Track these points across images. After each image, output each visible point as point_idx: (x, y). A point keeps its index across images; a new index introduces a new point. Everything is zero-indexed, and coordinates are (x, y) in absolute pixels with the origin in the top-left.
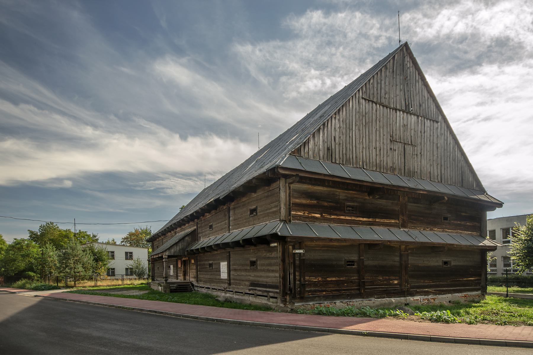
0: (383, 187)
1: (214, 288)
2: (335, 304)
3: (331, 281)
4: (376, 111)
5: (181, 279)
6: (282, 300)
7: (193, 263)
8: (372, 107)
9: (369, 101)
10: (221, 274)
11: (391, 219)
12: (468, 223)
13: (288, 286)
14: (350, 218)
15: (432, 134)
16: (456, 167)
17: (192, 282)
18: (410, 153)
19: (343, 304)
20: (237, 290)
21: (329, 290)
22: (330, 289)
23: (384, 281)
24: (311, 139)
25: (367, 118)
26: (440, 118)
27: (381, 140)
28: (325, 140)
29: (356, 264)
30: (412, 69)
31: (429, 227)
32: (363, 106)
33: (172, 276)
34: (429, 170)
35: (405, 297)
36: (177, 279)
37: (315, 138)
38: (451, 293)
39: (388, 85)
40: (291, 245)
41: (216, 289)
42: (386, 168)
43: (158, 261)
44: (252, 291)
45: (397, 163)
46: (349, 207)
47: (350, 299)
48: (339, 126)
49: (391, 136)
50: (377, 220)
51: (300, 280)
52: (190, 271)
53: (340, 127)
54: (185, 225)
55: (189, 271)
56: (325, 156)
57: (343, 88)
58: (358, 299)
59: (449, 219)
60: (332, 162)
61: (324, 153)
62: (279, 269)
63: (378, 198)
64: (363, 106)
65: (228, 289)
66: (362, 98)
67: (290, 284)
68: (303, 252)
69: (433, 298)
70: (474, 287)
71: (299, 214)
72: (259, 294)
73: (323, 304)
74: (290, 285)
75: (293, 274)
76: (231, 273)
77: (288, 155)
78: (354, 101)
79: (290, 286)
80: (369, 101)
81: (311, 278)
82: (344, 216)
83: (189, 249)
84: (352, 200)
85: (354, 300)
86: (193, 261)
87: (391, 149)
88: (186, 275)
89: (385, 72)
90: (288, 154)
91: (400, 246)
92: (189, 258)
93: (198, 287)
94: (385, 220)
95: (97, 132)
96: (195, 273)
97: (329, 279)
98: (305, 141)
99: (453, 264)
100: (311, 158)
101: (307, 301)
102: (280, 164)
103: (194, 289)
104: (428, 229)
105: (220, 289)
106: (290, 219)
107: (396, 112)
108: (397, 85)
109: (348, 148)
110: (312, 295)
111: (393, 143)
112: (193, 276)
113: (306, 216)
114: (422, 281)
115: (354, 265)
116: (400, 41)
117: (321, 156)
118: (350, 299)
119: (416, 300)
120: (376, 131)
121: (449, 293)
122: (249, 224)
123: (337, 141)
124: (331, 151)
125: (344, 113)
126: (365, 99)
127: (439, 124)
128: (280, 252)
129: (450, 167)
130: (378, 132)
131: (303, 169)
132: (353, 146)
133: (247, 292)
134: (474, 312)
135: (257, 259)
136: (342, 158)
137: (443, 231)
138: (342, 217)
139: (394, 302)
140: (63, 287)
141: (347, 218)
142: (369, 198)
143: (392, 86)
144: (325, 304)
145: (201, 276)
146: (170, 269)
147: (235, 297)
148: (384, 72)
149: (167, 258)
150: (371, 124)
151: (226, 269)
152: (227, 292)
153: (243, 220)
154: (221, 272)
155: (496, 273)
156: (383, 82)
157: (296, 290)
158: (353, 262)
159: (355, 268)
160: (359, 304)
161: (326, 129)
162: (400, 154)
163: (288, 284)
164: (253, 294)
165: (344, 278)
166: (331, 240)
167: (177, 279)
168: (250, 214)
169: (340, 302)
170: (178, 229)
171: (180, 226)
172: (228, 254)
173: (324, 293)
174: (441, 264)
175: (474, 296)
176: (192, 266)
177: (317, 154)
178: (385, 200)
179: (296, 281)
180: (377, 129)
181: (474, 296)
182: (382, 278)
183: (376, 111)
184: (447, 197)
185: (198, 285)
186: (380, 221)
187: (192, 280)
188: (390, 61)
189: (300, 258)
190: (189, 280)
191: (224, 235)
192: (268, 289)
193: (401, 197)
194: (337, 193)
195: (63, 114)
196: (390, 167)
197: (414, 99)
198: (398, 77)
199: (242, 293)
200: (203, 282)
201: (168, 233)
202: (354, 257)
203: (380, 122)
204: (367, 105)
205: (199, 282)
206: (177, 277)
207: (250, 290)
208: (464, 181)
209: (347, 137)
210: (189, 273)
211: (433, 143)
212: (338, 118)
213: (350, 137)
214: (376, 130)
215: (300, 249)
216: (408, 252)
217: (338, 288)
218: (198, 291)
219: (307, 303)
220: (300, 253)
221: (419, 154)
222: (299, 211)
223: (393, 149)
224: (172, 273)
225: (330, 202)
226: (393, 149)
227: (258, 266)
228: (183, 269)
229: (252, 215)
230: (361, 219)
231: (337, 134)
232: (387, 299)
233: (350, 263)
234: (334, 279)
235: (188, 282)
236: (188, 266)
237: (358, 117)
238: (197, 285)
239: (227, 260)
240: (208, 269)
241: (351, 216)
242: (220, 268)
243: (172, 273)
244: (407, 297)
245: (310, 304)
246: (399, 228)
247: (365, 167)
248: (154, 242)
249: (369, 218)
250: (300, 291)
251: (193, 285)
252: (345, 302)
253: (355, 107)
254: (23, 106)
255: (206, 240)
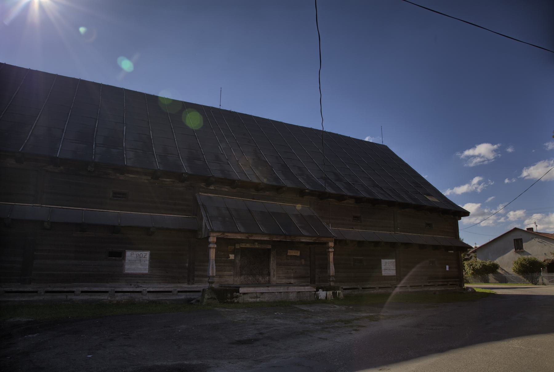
207: (429, 282)
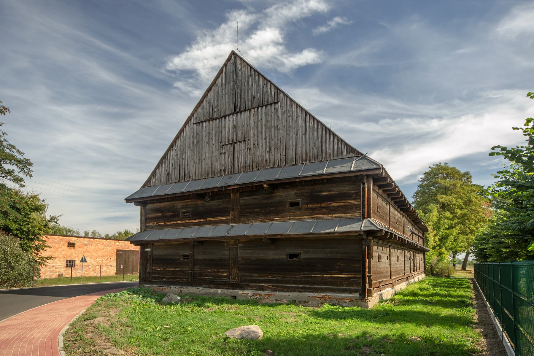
0: (193, 194)
3: (169, 270)
11: (222, 217)
12: (333, 204)
23: (211, 273)
31: (267, 218)
38: (299, 292)
50: (208, 220)
60: (169, 183)
63: (210, 200)
84: (187, 207)
95: (443, 122)
97: (167, 269)
99: (303, 256)
101: (153, 284)
114: (257, 275)
118: (182, 285)
119: (245, 294)
134: (127, 302)
137: (289, 219)
138: (179, 222)
140: (519, 265)
141: (183, 222)
174: (284, 257)
175: (339, 299)
178: (216, 201)
181: (339, 299)
184: (267, 184)
194: (176, 205)
195: (410, 116)
202: (187, 252)
216: (237, 245)
217: (174, 277)
222: (151, 222)
225: (171, 212)
230: (194, 221)
232: (214, 289)
233: (186, 257)
234: (171, 269)
241: (185, 220)
249: (200, 219)
254: (382, 122)
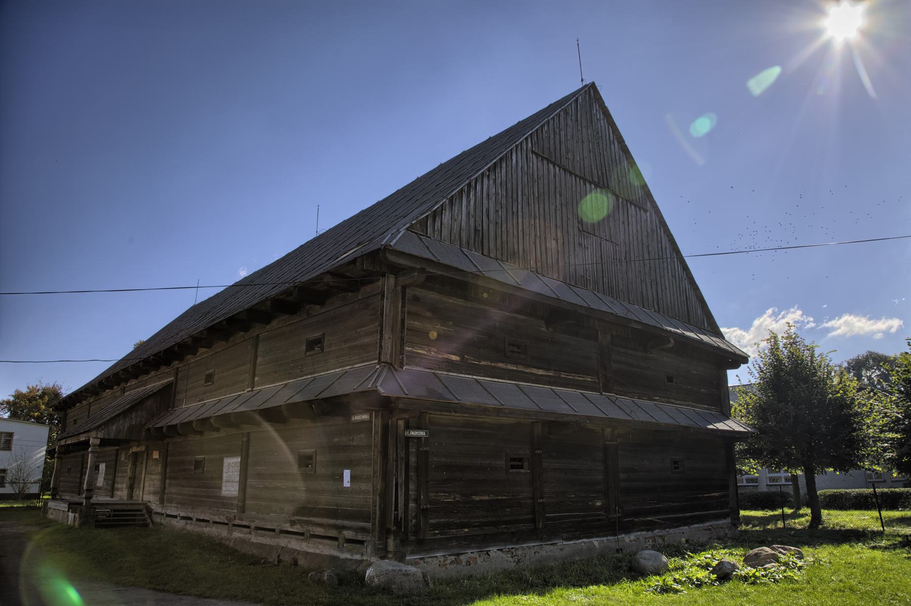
1: (202, 518)
2: (487, 556)
3: (481, 501)
4: (555, 177)
5: (122, 494)
6: (378, 548)
7: (157, 459)
8: (548, 169)
9: (543, 158)
10: (224, 484)
12: (702, 390)
13: (393, 512)
14: (515, 368)
15: (639, 229)
16: (678, 289)
17: (149, 504)
18: (610, 255)
19: (503, 555)
20: (261, 524)
21: (477, 524)
22: (478, 520)
24: (446, 206)
25: (541, 186)
26: (649, 204)
27: (565, 227)
28: (472, 212)
29: (526, 464)
30: (603, 123)
32: (533, 165)
33: (99, 488)
34: (641, 290)
35: (615, 535)
36: (112, 497)
37: (453, 207)
39: (570, 138)
40: (402, 419)
41: (208, 521)
42: (574, 279)
43: (72, 454)
44: (299, 527)
45: (591, 270)
46: (513, 345)
47: (517, 543)
48: (496, 191)
49: (579, 223)
51: (416, 501)
52: (146, 479)
53: (496, 194)
54: (147, 372)
55: (143, 478)
56: (472, 241)
57: (487, 140)
58: (533, 542)
59: (674, 380)
61: (469, 236)
62: (372, 473)
64: (533, 165)
65: (237, 522)
66: (533, 152)
67: (396, 509)
68: (426, 435)
69: (662, 535)
70: (720, 510)
71: (418, 351)
72: (318, 534)
73: (464, 555)
74: (397, 511)
75: (403, 486)
76: (248, 483)
77: (404, 231)
78: (520, 154)
79: (398, 514)
80: (543, 158)
81: (440, 494)
82: (503, 362)
83: (150, 425)
85: (523, 546)
86: (156, 455)
87: (580, 245)
88: (136, 485)
89: (566, 119)
90: (405, 228)
91: (602, 429)
92: (147, 447)
93: (163, 516)
94: (576, 375)
96: (157, 483)
98: (436, 208)
100: (445, 241)
102: (392, 244)
103: (152, 521)
104: (645, 398)
105: (218, 520)
106: (403, 360)
107: (585, 184)
108: (583, 142)
109: (511, 231)
110: (441, 535)
111: (582, 235)
112: (152, 489)
113: (432, 356)
115: (522, 467)
116: (582, 80)
117: (464, 241)
118: (517, 543)
120: (556, 210)
121: (685, 525)
122: (302, 371)
123: (491, 217)
124: (481, 233)
125: (504, 171)
126: (537, 155)
127: (648, 213)
128: (376, 433)
129: (669, 287)
130: (558, 212)
131: (435, 260)
132: (519, 231)
133: (286, 529)
135: (316, 451)
136: (500, 249)
139: (597, 546)
141: (510, 367)
142: (548, 330)
143: (577, 142)
144: (469, 556)
145: (173, 490)
146: (97, 472)
147: (255, 541)
148: (564, 118)
149: (98, 446)
150: (546, 197)
151: (236, 473)
152: (233, 528)
153: (289, 362)
154: (224, 479)
155: (757, 486)
156: (563, 133)
157: (408, 523)
158: (520, 460)
159: (525, 474)
160: (535, 553)
161: (472, 194)
162: (594, 255)
163: (393, 509)
164: (302, 534)
165: (504, 496)
166: (485, 411)
167: (112, 497)
168: (307, 350)
169: (498, 550)
170: (133, 382)
171: (136, 377)
172: (245, 439)
173: (466, 530)
176: (152, 465)
177: (457, 235)
179: (408, 504)
180: (556, 207)
182: (573, 496)
183: (555, 177)
184: (675, 340)
185: (163, 512)
186: (567, 377)
187: (147, 498)
188: (572, 103)
189: (418, 450)
190: (142, 498)
191: (240, 395)
192: (339, 522)
193: (601, 334)
196: (580, 277)
197: (609, 168)
198: (584, 130)
199: (273, 530)
200: (176, 503)
201: (105, 391)
203: (561, 195)
204: (539, 164)
205: (165, 504)
206: (112, 491)
207: (293, 523)
208: (690, 313)
209: (508, 213)
210: (142, 482)
211: (643, 244)
212: (494, 177)
213: (513, 213)
214: (555, 208)
215: (419, 428)
218: (162, 524)
219: (434, 553)
220: (419, 438)
221: (623, 259)
223: (583, 245)
224: (100, 481)
226: (583, 245)
227: (317, 467)
228: (129, 473)
229: (312, 353)
230: (535, 371)
231: (492, 205)
232: (585, 540)
235: (140, 504)
236: (144, 465)
237: (526, 181)
238: (159, 510)
239: (241, 451)
240: (192, 473)
242: (222, 470)
243: (100, 481)
244: (620, 534)
245: (437, 557)
246: (600, 392)
247: (540, 270)
248: (69, 411)
250: (417, 525)
251: (150, 511)
252: (507, 550)
253: (520, 164)
255: (194, 405)
